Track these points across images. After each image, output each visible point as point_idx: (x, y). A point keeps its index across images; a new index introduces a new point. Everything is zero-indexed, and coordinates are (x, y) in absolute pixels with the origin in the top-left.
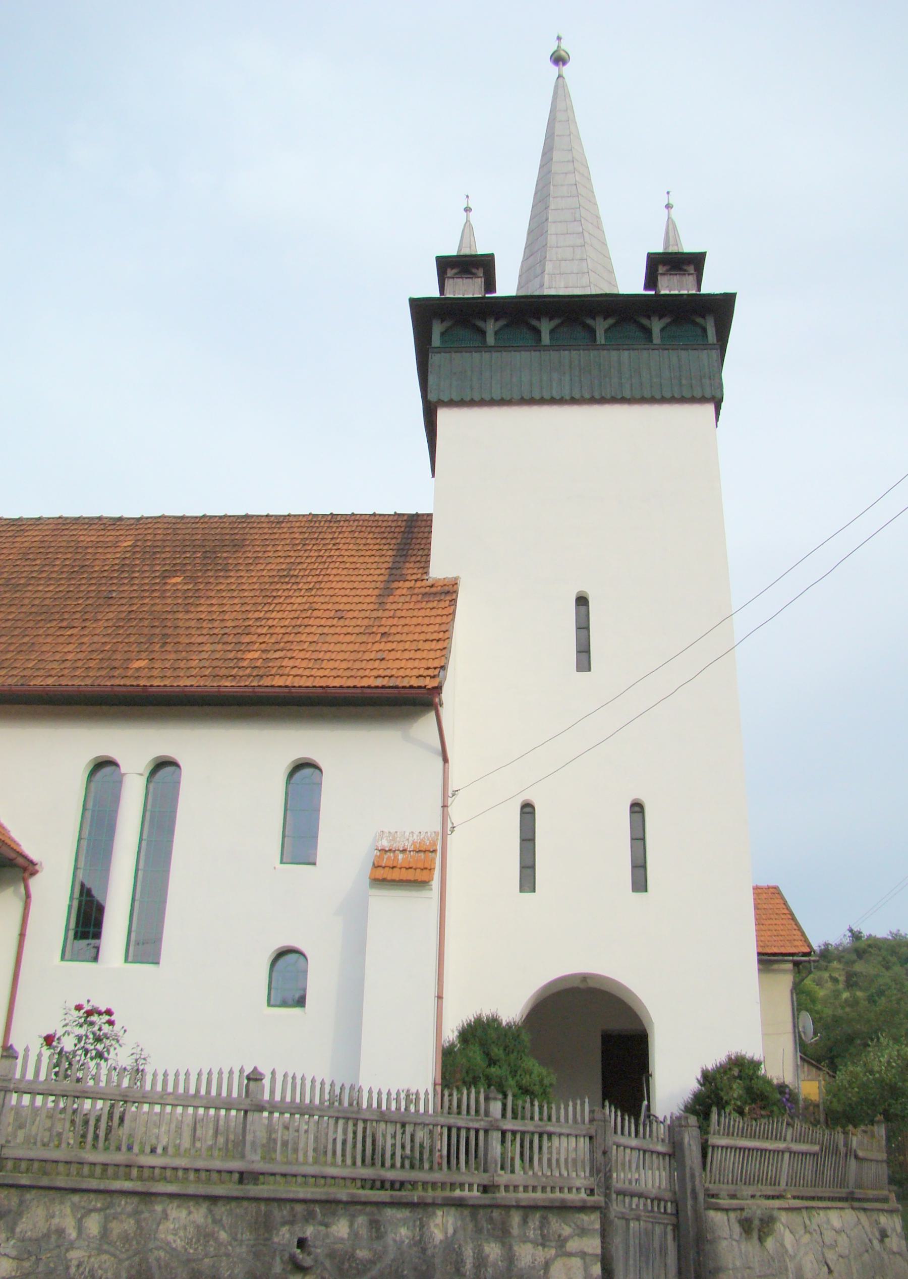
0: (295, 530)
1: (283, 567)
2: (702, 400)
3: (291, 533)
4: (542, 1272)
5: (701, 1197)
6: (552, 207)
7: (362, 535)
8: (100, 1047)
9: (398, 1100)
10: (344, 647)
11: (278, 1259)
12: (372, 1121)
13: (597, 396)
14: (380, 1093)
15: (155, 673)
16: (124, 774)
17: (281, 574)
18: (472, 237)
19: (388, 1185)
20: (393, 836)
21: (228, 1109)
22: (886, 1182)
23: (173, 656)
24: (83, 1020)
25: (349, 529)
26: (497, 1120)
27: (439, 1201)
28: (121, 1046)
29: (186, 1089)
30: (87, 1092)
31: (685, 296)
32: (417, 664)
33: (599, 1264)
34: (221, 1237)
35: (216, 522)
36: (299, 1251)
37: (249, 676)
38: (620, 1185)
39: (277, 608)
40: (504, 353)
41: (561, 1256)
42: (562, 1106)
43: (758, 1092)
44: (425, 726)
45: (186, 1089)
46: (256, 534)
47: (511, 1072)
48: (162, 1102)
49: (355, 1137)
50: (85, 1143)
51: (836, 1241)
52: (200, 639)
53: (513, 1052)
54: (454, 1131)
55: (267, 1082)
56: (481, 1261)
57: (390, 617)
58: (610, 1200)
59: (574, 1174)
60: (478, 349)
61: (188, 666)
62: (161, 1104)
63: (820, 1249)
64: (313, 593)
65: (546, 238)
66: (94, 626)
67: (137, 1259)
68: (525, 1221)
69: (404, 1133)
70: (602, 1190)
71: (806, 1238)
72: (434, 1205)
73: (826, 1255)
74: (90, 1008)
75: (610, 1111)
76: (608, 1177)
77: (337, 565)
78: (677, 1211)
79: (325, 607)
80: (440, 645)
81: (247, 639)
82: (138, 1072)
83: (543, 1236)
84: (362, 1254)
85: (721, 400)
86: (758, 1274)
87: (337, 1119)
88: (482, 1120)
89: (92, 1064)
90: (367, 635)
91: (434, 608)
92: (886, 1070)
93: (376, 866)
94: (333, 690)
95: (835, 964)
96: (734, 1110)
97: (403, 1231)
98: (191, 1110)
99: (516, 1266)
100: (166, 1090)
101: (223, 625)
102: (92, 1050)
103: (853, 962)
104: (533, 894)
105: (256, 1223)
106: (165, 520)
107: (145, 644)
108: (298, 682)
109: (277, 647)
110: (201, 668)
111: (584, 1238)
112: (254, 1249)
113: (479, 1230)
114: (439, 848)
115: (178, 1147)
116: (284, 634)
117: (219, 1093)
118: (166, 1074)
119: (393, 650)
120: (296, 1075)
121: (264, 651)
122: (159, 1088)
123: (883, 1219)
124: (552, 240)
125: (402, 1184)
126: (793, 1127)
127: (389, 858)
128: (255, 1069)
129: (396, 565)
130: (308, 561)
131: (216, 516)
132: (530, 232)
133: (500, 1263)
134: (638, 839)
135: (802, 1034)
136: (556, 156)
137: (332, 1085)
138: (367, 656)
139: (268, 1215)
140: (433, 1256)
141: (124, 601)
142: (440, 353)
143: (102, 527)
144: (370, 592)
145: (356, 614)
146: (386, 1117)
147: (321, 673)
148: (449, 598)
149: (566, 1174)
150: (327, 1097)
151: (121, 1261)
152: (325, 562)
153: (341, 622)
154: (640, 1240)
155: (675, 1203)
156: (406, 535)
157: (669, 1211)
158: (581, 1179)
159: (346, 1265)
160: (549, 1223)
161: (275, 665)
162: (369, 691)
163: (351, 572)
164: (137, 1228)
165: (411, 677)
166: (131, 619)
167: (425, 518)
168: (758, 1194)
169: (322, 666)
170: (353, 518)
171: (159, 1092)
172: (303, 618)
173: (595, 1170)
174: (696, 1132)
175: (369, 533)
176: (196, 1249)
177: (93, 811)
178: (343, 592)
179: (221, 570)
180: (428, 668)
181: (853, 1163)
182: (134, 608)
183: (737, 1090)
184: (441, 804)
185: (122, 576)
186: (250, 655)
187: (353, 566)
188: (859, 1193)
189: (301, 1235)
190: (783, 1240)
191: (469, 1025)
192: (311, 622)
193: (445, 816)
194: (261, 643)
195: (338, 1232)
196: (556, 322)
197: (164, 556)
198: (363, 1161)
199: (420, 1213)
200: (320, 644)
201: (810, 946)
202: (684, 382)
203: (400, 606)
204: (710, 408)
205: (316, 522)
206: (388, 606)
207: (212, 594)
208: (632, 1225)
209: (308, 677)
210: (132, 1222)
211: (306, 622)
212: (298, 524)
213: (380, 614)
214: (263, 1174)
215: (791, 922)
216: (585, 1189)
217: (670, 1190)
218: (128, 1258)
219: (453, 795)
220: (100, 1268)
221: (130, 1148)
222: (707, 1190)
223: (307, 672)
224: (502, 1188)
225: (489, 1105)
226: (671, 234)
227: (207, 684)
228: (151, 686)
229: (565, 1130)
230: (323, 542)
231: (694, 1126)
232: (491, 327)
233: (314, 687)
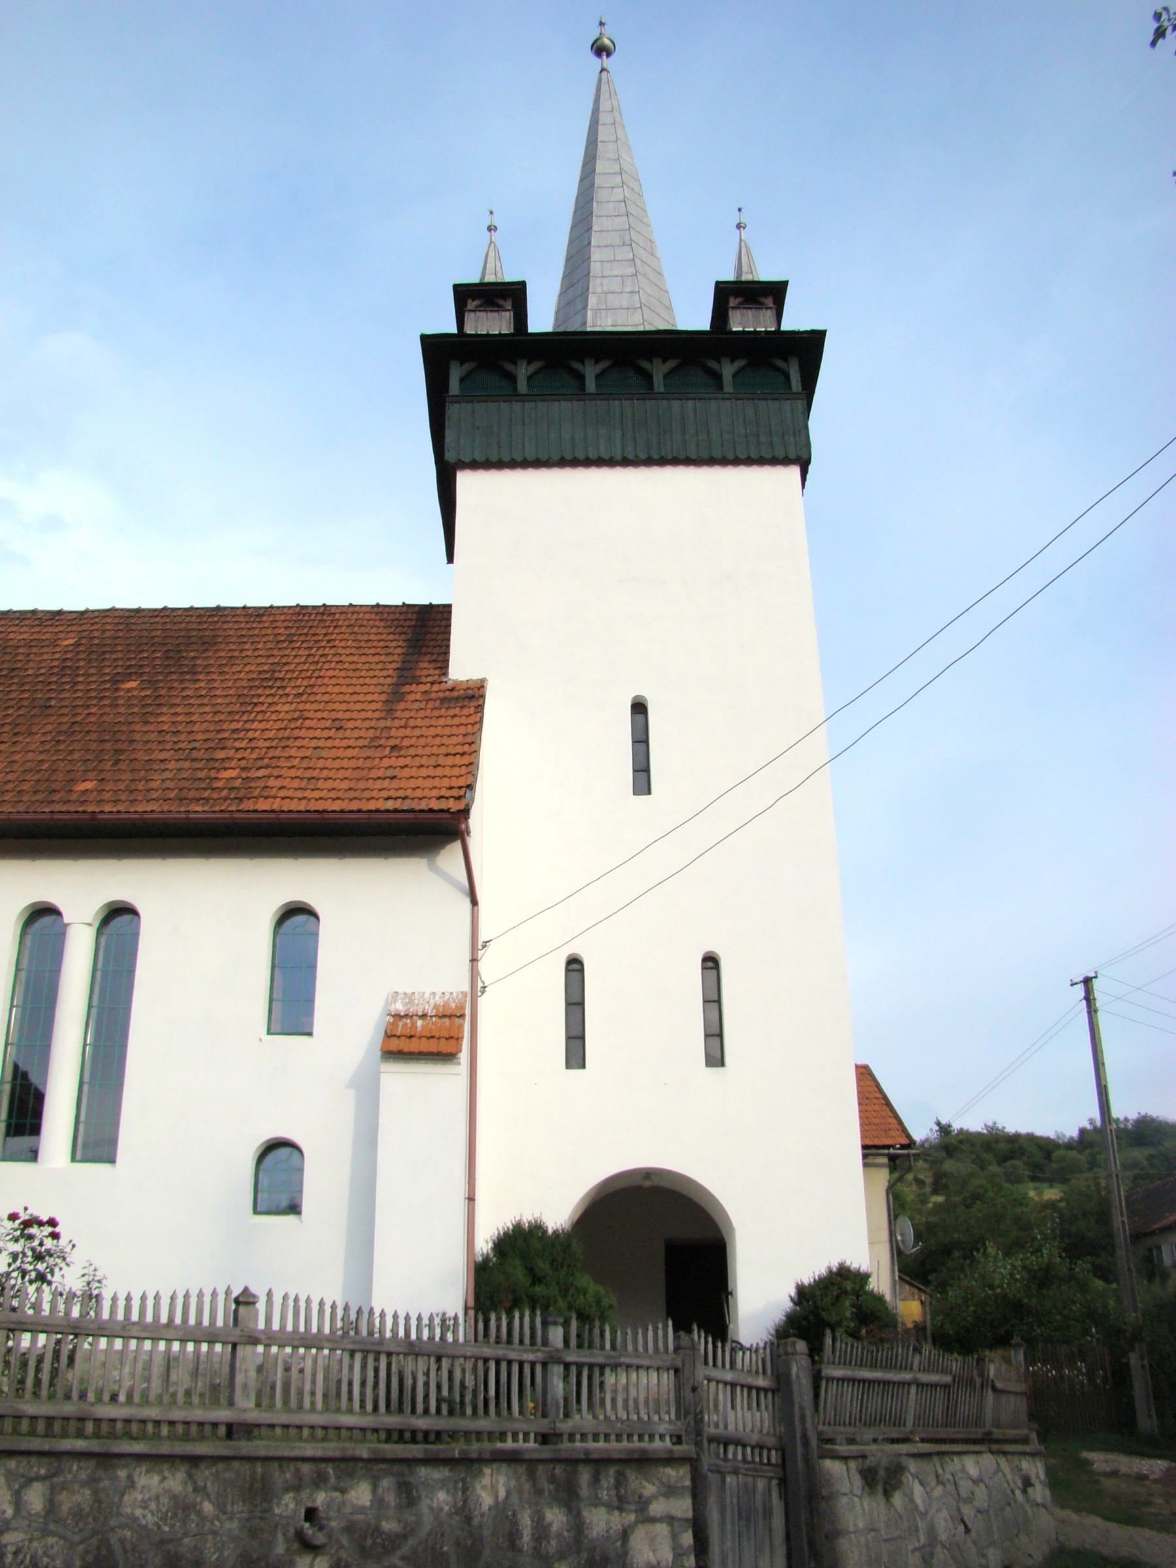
0: (279, 624)
1: (266, 668)
2: (786, 461)
3: (274, 628)
4: (619, 1544)
5: (814, 1442)
6: (595, 228)
7: (363, 630)
8: (41, 1266)
9: (431, 1326)
10: (345, 763)
11: (280, 1537)
12: (398, 1354)
13: (656, 457)
14: (407, 1318)
15: (107, 796)
16: (69, 924)
17: (263, 677)
18: (498, 262)
19: (420, 1436)
20: (409, 997)
21: (211, 1342)
22: (1026, 1419)
23: (128, 776)
24: (19, 1232)
25: (346, 623)
26: (557, 1350)
27: (487, 1456)
28: (68, 1265)
29: (156, 1316)
30: (25, 1323)
31: (763, 334)
32: (437, 782)
34: (206, 1510)
35: (181, 616)
36: (307, 1525)
37: (225, 799)
38: (712, 1430)
39: (260, 717)
40: (540, 404)
41: (643, 1522)
42: (640, 1331)
43: (868, 1311)
44: (451, 857)
45: (156, 1316)
46: (230, 629)
47: (560, 1291)
48: (126, 1334)
49: (376, 1376)
50: (23, 1390)
51: (973, 1494)
52: (162, 756)
53: (562, 1267)
54: (504, 1366)
55: (261, 1306)
56: (541, 1531)
57: (402, 727)
58: (701, 1448)
59: (656, 1418)
61: (147, 788)
62: (123, 1337)
63: (955, 1503)
64: (304, 698)
65: (590, 264)
66: (28, 740)
67: (94, 1541)
68: (596, 1480)
69: (439, 1368)
70: (693, 1436)
71: (938, 1491)
73: (963, 1510)
74: (27, 1217)
75: (699, 1337)
76: (699, 1420)
77: (333, 665)
78: (784, 1460)
79: (319, 715)
80: (466, 760)
81: (221, 755)
82: (91, 1298)
83: (620, 1498)
84: (388, 1526)
85: (808, 462)
86: (885, 1537)
87: (352, 1353)
88: (538, 1350)
89: (32, 1289)
90: (373, 749)
91: (455, 716)
92: (1009, 1284)
93: (389, 1035)
94: (332, 815)
96: (846, 1332)
97: (442, 1495)
98: (162, 1345)
99: (586, 1537)
100: (130, 1319)
101: (191, 738)
102: (30, 1271)
104: (582, 1070)
105: (251, 1489)
106: (116, 614)
107: (93, 762)
108: (288, 805)
109: (260, 763)
110: (164, 790)
111: (671, 1499)
112: (248, 1524)
113: (539, 1492)
114: (468, 1012)
115: (145, 1394)
116: (268, 748)
118: (129, 1298)
119: (406, 766)
120: (300, 1296)
121: (243, 769)
122: (120, 1316)
123: (1025, 1464)
124: (595, 268)
125: (438, 1434)
126: (920, 1353)
128: (246, 1289)
129: (407, 665)
130: (297, 660)
131: (180, 609)
132: (569, 259)
133: (566, 1533)
134: (713, 1000)
135: (900, 1244)
136: (600, 167)
137: (346, 1308)
140: (481, 1526)
141: (65, 711)
142: (460, 402)
143: (37, 622)
144: (375, 697)
145: (358, 723)
146: (417, 1349)
147: (316, 794)
148: (474, 703)
149: (646, 1418)
150: (339, 1324)
151: (73, 1545)
152: (317, 663)
153: (340, 734)
154: (739, 1498)
155: (782, 1451)
156: (418, 630)
157: (773, 1461)
158: (666, 1422)
159: (369, 1542)
161: (257, 785)
162: (378, 815)
163: (350, 674)
164: (94, 1501)
165: (430, 798)
166: (75, 731)
167: (441, 609)
168: (881, 1437)
169: (318, 786)
170: (352, 609)
171: (120, 1321)
172: (292, 729)
173: (682, 1410)
174: (805, 1361)
175: (372, 627)
176: (172, 1526)
177: (29, 971)
178: (341, 698)
179: (188, 673)
180: (451, 788)
181: (990, 1396)
182: (79, 718)
183: (847, 1309)
185: (63, 680)
187: (353, 666)
188: (997, 1433)
189: (310, 1505)
190: (912, 1493)
192: (303, 733)
193: (474, 974)
194: (239, 760)
195: (358, 1499)
197: (115, 656)
198: (388, 1406)
200: (314, 760)
201: (908, 1136)
203: (413, 714)
204: (795, 471)
205: (304, 615)
206: (398, 714)
207: (177, 701)
208: (728, 1480)
209: (300, 799)
210: (88, 1492)
211: (296, 733)
212: (283, 617)
213: (389, 723)
214: (258, 1426)
216: (671, 1436)
217: (774, 1435)
218: (82, 1542)
219: (484, 947)
220: (45, 1554)
221: (83, 1396)
222: (820, 1434)
223: (299, 794)
224: (566, 1437)
225: (548, 1332)
226: (744, 260)
227: (172, 809)
228: (101, 812)
229: (646, 1362)
230: (314, 638)
231: (802, 1354)
232: (523, 371)
233: (309, 811)
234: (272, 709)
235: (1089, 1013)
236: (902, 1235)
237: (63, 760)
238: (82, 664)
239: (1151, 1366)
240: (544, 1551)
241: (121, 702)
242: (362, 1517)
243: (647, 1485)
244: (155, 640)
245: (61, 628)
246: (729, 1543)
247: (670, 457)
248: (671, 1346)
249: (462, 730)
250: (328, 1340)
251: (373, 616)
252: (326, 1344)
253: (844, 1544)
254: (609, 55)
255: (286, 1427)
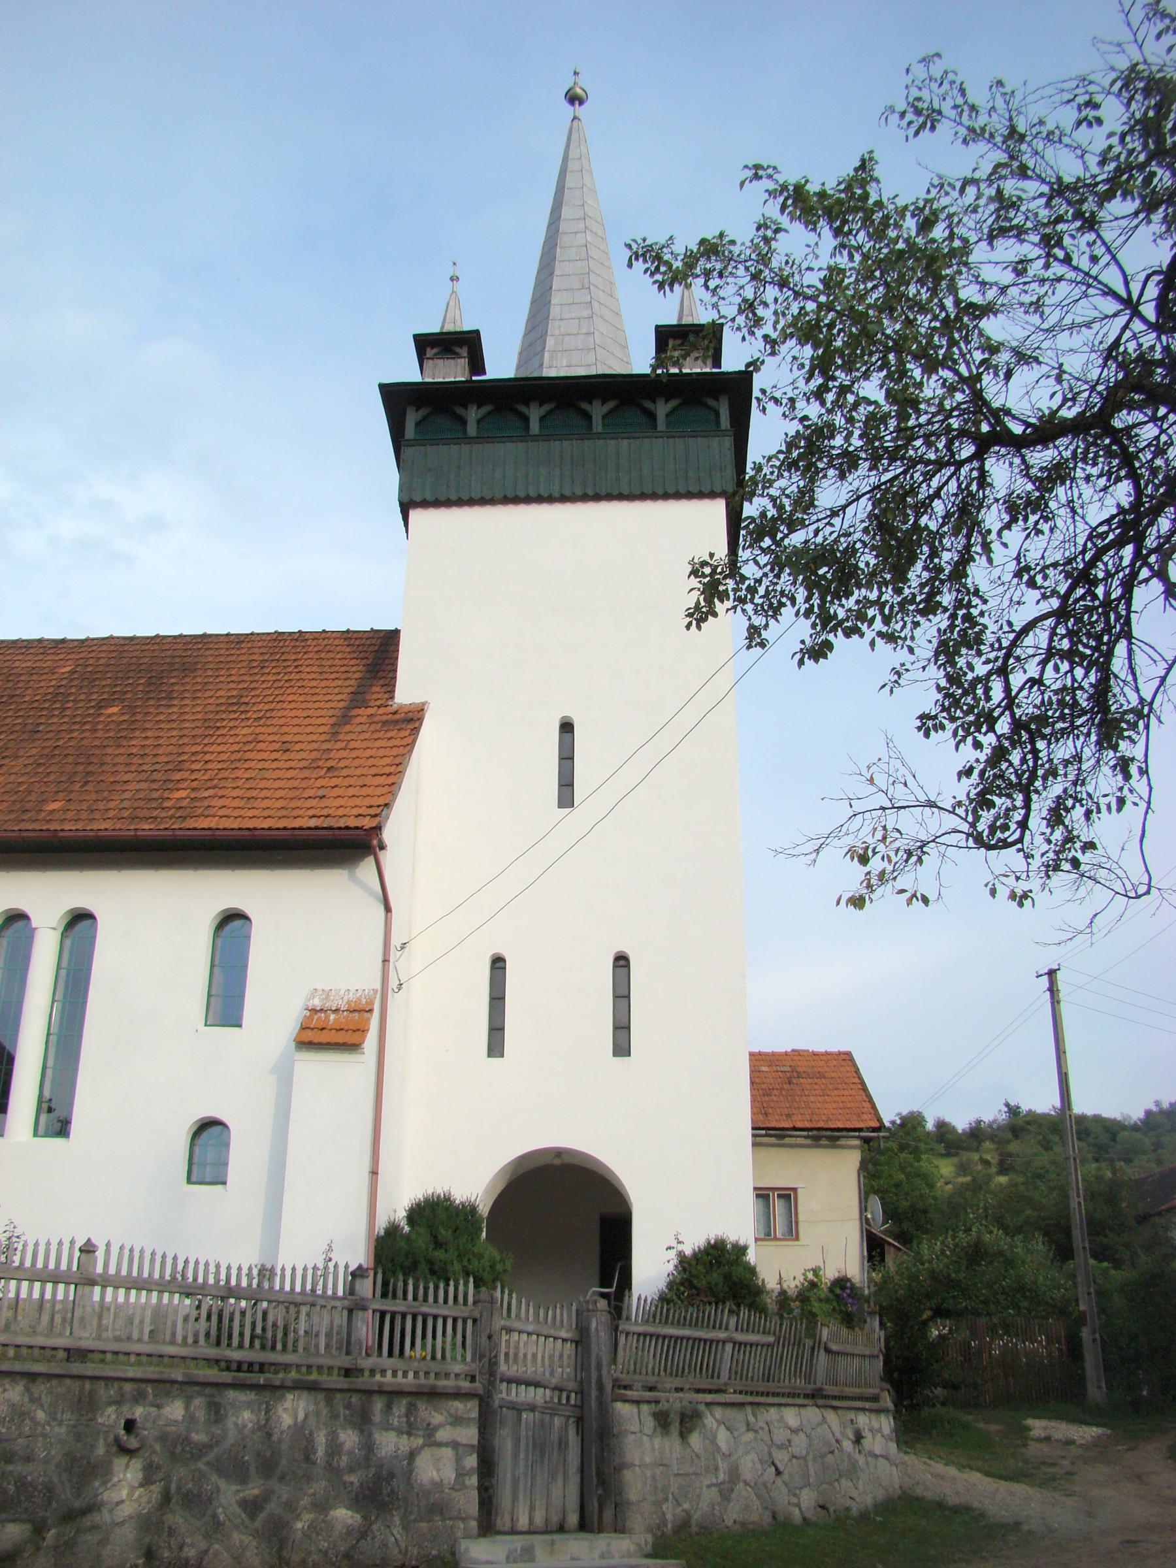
0: (255, 650)
1: (235, 693)
4: (405, 1462)
6: (557, 272)
9: (249, 1275)
11: (101, 1442)
13: (591, 493)
15: (70, 815)
20: (327, 994)
27: (289, 1384)
32: (358, 801)
33: (475, 1455)
37: (171, 818)
41: (429, 1446)
44: (366, 869)
51: (789, 1441)
52: (126, 778)
54: (440, 1322)
55: (100, 1254)
56: (334, 1448)
60: (456, 441)
64: (262, 722)
68: (389, 1407)
72: (283, 1388)
73: (774, 1455)
76: (493, 1364)
79: (271, 738)
81: (178, 776)
84: (198, 1437)
93: (304, 1028)
95: (988, 1144)
97: (247, 1415)
99: (375, 1455)
101: (156, 760)
103: (1008, 1142)
109: (209, 784)
117: (118, 1270)
121: (194, 789)
123: (862, 1420)
124: (555, 311)
126: (738, 1315)
127: (319, 1018)
128: (89, 1240)
129: (360, 689)
130: (264, 686)
132: (533, 302)
134: (622, 995)
136: (566, 213)
138: (306, 794)
139: (92, 1393)
143: (41, 651)
148: (411, 726)
153: (286, 756)
157: (573, 1402)
159: (179, 1449)
160: (416, 1408)
162: (300, 832)
168: (688, 1386)
170: (323, 635)
174: (605, 1318)
176: (9, 1429)
180: (371, 807)
182: (61, 743)
184: (380, 959)
186: (178, 795)
188: (830, 1389)
191: (418, 1205)
196: (547, 407)
197: (104, 683)
199: (267, 1394)
201: (880, 1120)
202: (690, 474)
203: (354, 736)
206: (341, 737)
208: (524, 1415)
214: (92, 1351)
215: (862, 1093)
222: (615, 1380)
223: (236, 813)
224: (367, 1373)
228: (62, 830)
232: (473, 414)
234: (232, 732)
235: (1052, 1003)
236: (872, 1213)
237: (38, 782)
238: (73, 690)
239: (1103, 1341)
240: (335, 1465)
241: (100, 727)
242: (174, 1429)
243: (436, 1415)
244: (142, 667)
245: (61, 656)
246: (522, 1470)
247: (603, 493)
248: (471, 1299)
249: (395, 752)
250: (157, 1283)
251: (341, 642)
252: (153, 1287)
253: (628, 1475)
254: (581, 103)
255: (116, 1353)
